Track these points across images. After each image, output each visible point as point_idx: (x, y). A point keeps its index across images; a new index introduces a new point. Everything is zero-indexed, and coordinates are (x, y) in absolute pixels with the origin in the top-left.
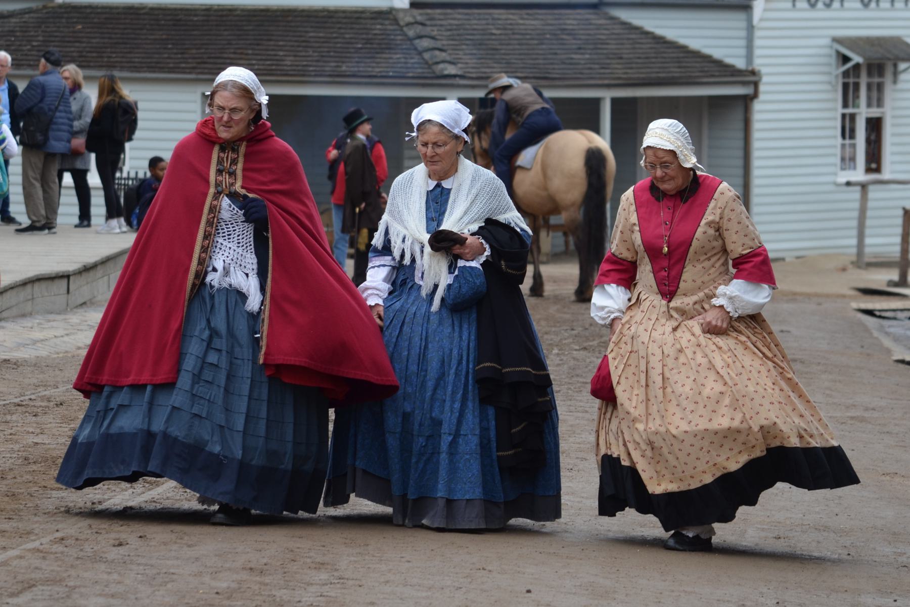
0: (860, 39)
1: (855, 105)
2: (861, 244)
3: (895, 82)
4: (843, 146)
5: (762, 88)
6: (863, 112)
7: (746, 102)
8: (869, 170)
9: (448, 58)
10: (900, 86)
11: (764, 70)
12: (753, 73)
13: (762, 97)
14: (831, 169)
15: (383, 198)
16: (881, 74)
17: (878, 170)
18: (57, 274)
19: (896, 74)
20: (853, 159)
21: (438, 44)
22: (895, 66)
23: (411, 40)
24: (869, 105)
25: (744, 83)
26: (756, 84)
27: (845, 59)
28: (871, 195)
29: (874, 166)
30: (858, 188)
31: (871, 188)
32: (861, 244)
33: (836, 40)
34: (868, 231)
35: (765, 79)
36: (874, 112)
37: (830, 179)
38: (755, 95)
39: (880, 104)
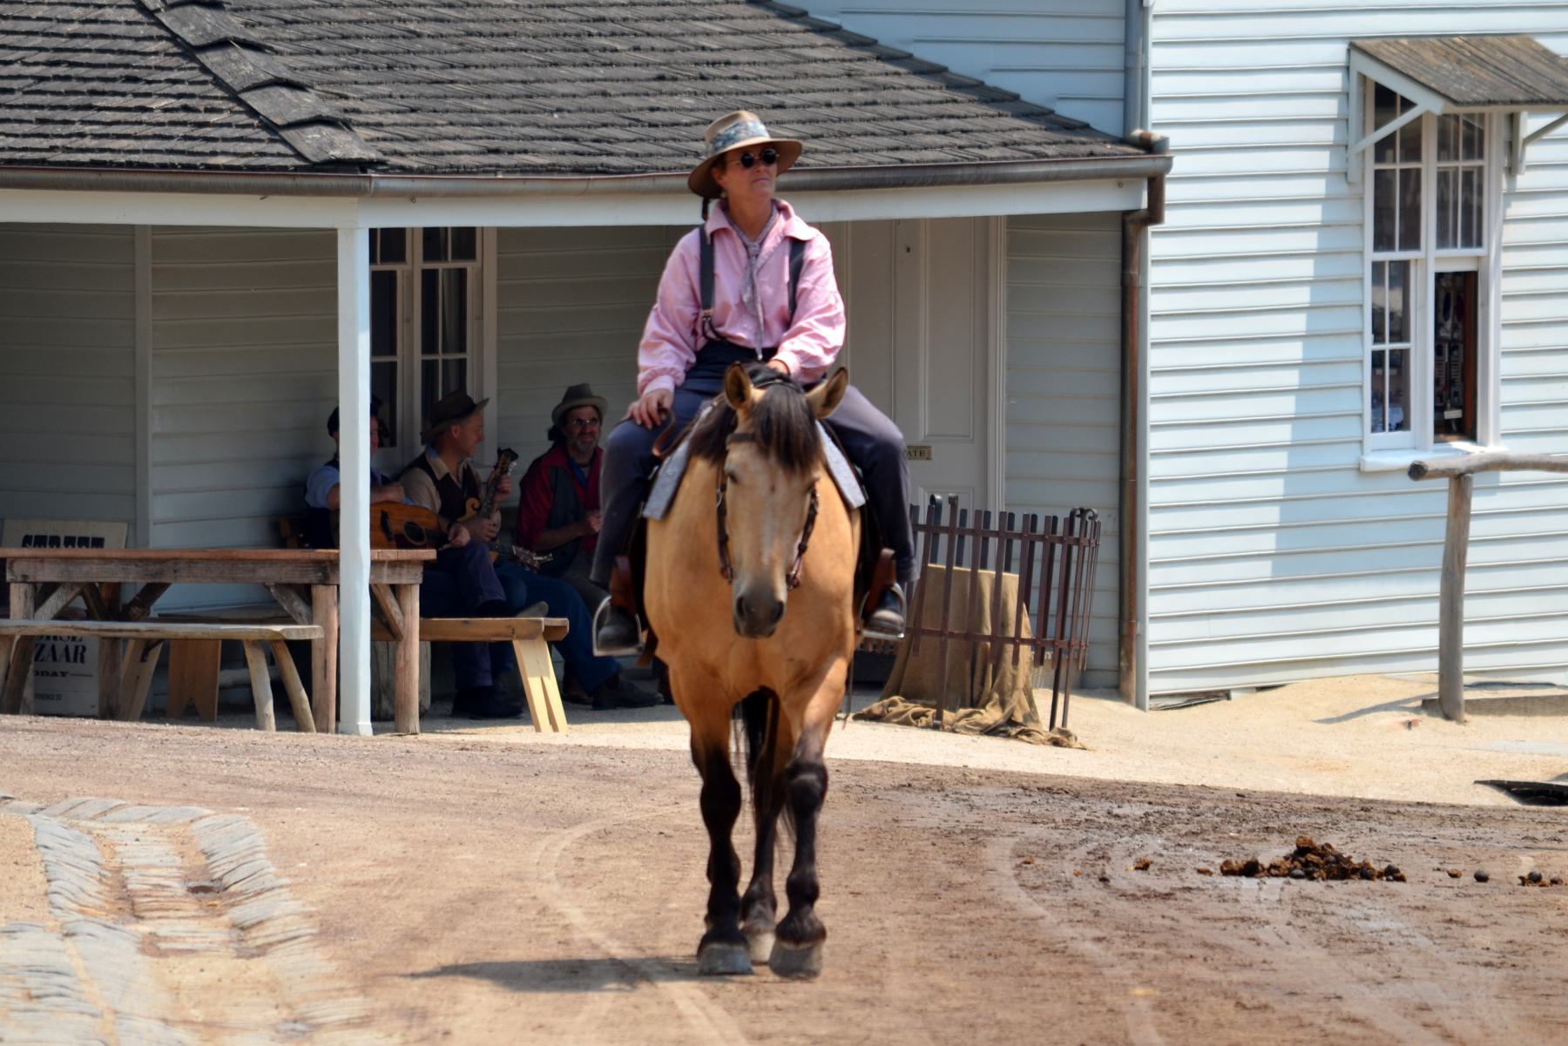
0: (1444, 42)
1: (1411, 240)
2: (1450, 651)
3: (1511, 170)
4: (1377, 359)
5: (1171, 192)
6: (1432, 259)
7: (1129, 231)
8: (1444, 428)
9: (325, 110)
10: (1525, 180)
11: (1176, 138)
12: (1149, 146)
13: (1171, 218)
14: (1351, 429)
15: (873, 451)
16: (1474, 144)
17: (1466, 428)
18: (1546, 459)
19: (1512, 147)
20: (1400, 396)
21: (279, 66)
22: (1513, 120)
23: (189, 51)
24: (1443, 240)
25: (1121, 178)
26: (1156, 186)
27: (1386, 101)
28: (1478, 503)
29: (1453, 414)
30: (1444, 483)
31: (1478, 480)
32: (1450, 651)
33: (1355, 47)
34: (1470, 608)
35: (1181, 165)
36: (1457, 259)
37: (1346, 457)
38: (1154, 213)
39: (1473, 235)
